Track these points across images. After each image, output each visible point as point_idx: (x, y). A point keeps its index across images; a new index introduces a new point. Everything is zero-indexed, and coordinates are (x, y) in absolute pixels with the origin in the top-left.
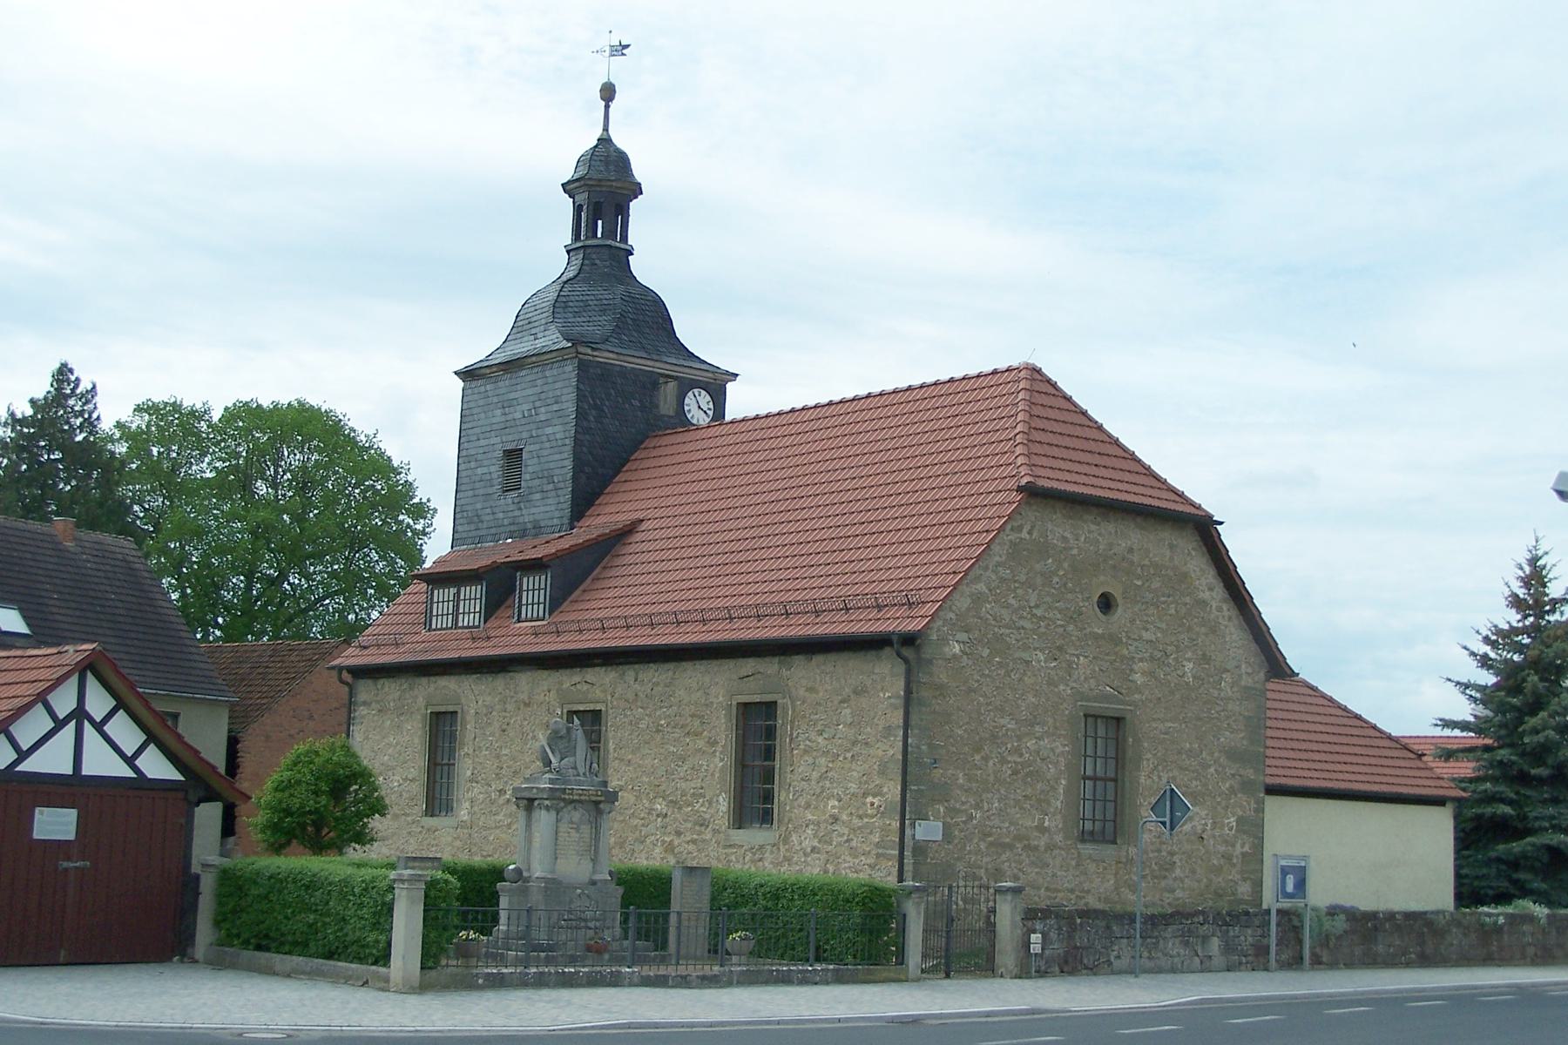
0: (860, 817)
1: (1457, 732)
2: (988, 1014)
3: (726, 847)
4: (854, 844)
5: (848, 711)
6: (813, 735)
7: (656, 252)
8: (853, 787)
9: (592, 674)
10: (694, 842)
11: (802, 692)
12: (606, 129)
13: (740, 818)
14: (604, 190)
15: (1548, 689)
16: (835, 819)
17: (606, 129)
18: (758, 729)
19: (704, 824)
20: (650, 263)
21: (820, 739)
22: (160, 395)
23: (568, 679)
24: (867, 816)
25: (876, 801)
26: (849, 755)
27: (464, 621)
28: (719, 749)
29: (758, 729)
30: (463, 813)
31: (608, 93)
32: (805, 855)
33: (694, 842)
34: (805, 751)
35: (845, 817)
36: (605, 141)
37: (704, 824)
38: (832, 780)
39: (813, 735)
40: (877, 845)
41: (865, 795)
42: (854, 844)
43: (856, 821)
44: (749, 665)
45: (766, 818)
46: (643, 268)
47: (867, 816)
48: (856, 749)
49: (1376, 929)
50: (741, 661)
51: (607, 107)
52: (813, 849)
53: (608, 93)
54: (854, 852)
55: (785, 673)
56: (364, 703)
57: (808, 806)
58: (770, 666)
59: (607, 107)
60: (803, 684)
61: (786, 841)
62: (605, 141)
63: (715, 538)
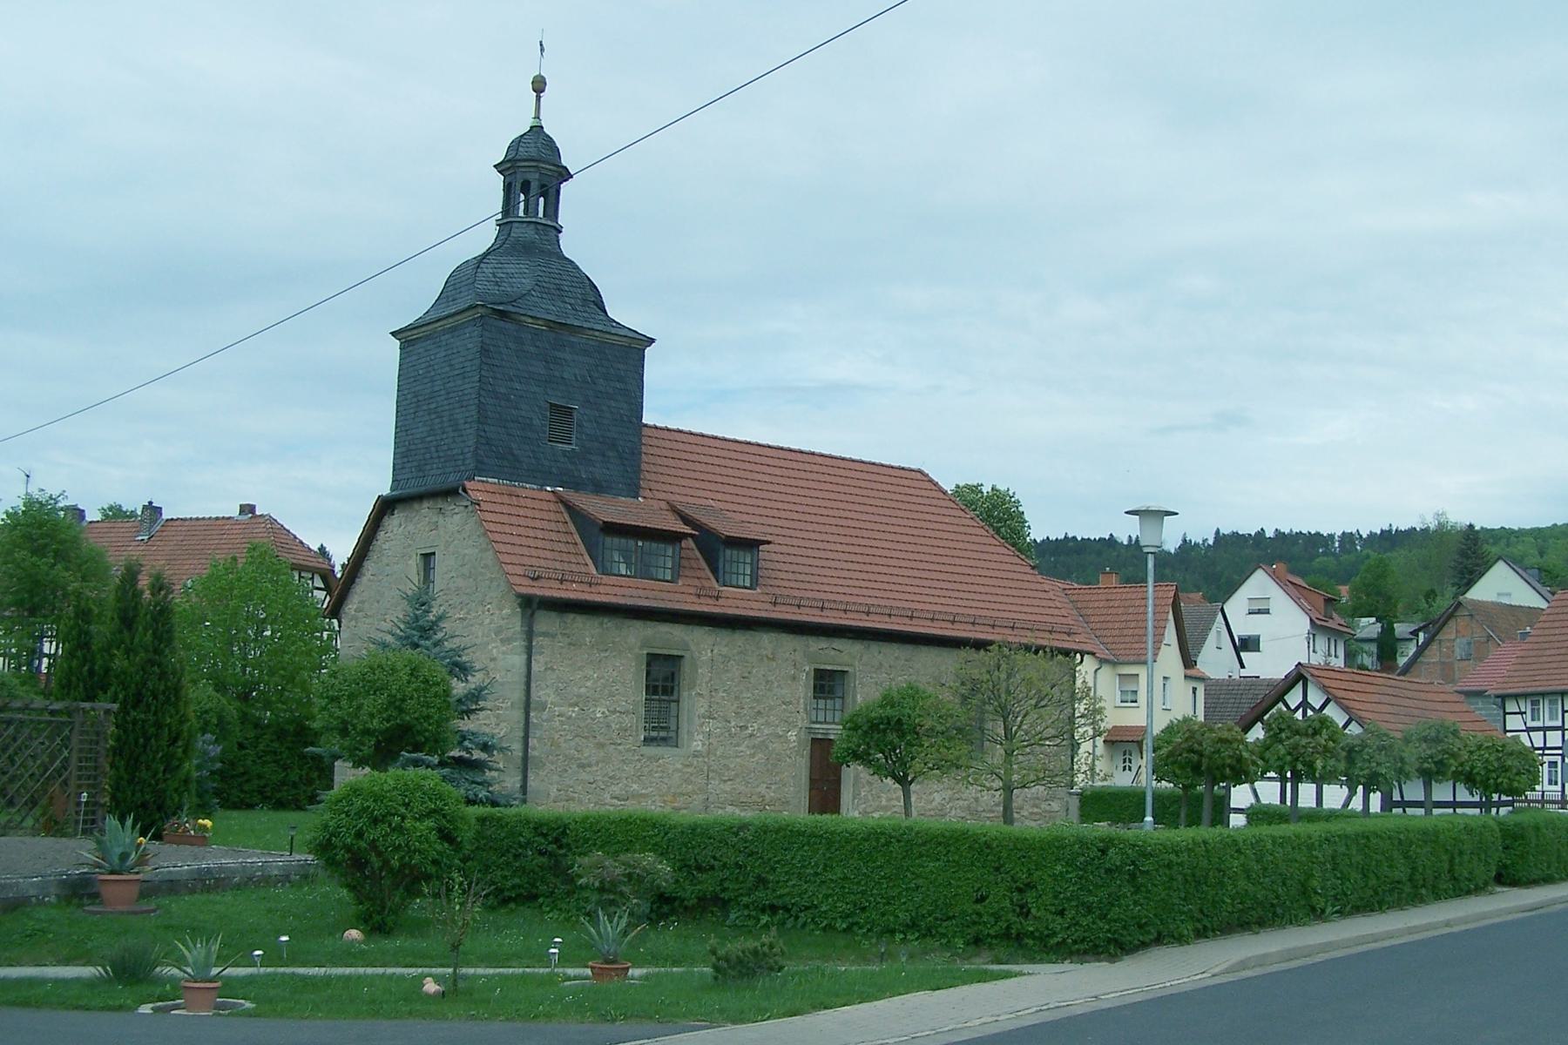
2: (1448, 924)
7: (585, 232)
9: (838, 644)
12: (537, 117)
14: (534, 171)
15: (971, 691)
17: (537, 117)
18: (663, 678)
20: (580, 241)
23: (816, 645)
29: (663, 678)
30: (697, 745)
31: (539, 86)
36: (537, 130)
46: (569, 245)
49: (444, 923)
51: (538, 98)
53: (539, 86)
56: (545, 634)
59: (538, 98)
62: (537, 130)
63: (865, 534)
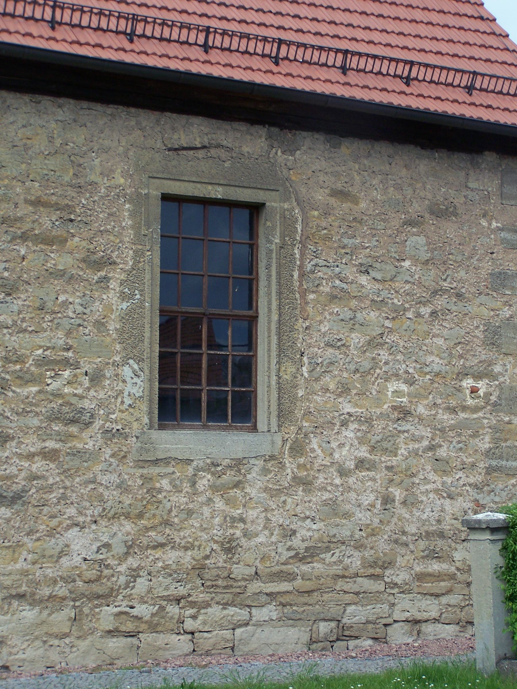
0: (453, 410)
1: (215, 239)
3: (141, 463)
4: (442, 453)
5: (421, 240)
6: (350, 273)
8: (436, 363)
10: (50, 455)
11: (320, 196)
13: (175, 405)
16: (404, 413)
19: (79, 419)
21: (363, 280)
22: (497, 119)
24: (464, 408)
25: (482, 386)
26: (426, 311)
27: (239, 136)
28: (117, 276)
32: (343, 473)
33: (50, 455)
34: (333, 298)
35: (421, 410)
37: (79, 419)
38: (392, 349)
39: (350, 273)
40: (488, 454)
41: (463, 374)
42: (442, 453)
43: (446, 418)
44: (194, 130)
45: (236, 408)
47: (464, 408)
48: (441, 302)
50: (169, 119)
52: (361, 464)
54: (442, 466)
55: (280, 157)
57: (344, 390)
58: (251, 143)
60: (311, 176)
61: (298, 449)
